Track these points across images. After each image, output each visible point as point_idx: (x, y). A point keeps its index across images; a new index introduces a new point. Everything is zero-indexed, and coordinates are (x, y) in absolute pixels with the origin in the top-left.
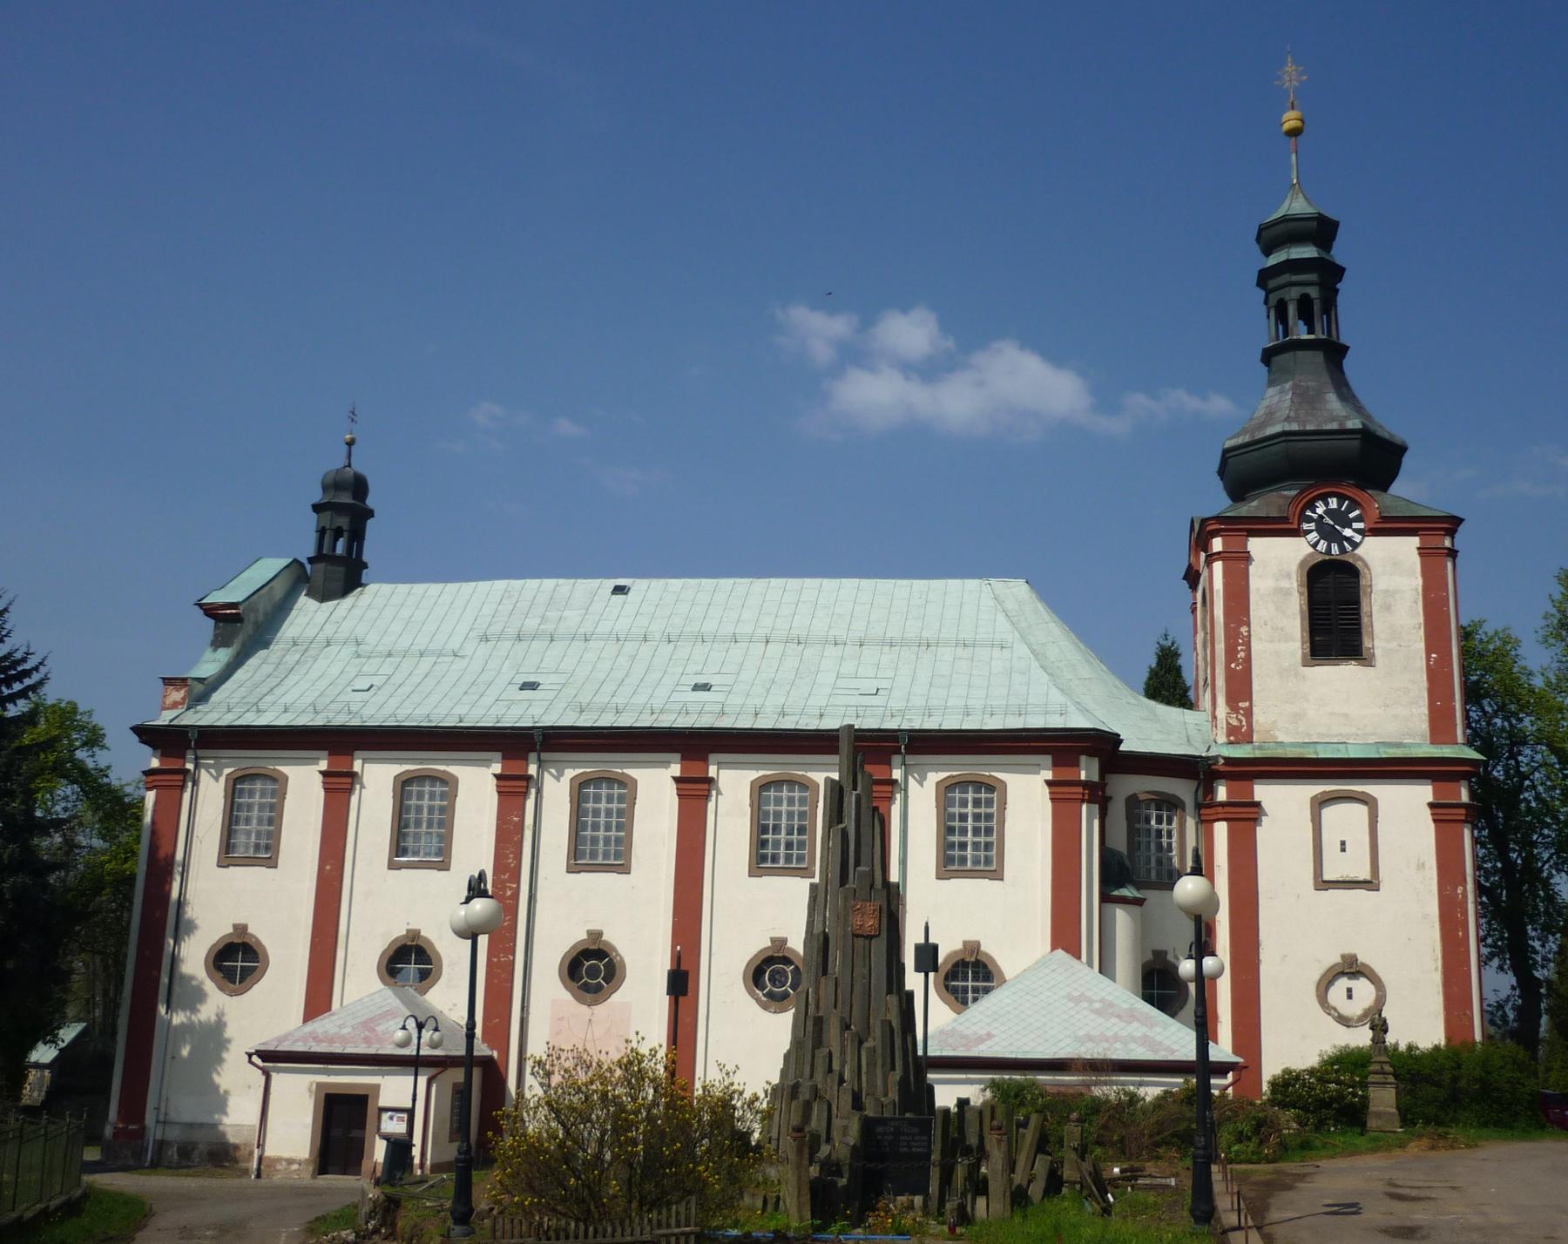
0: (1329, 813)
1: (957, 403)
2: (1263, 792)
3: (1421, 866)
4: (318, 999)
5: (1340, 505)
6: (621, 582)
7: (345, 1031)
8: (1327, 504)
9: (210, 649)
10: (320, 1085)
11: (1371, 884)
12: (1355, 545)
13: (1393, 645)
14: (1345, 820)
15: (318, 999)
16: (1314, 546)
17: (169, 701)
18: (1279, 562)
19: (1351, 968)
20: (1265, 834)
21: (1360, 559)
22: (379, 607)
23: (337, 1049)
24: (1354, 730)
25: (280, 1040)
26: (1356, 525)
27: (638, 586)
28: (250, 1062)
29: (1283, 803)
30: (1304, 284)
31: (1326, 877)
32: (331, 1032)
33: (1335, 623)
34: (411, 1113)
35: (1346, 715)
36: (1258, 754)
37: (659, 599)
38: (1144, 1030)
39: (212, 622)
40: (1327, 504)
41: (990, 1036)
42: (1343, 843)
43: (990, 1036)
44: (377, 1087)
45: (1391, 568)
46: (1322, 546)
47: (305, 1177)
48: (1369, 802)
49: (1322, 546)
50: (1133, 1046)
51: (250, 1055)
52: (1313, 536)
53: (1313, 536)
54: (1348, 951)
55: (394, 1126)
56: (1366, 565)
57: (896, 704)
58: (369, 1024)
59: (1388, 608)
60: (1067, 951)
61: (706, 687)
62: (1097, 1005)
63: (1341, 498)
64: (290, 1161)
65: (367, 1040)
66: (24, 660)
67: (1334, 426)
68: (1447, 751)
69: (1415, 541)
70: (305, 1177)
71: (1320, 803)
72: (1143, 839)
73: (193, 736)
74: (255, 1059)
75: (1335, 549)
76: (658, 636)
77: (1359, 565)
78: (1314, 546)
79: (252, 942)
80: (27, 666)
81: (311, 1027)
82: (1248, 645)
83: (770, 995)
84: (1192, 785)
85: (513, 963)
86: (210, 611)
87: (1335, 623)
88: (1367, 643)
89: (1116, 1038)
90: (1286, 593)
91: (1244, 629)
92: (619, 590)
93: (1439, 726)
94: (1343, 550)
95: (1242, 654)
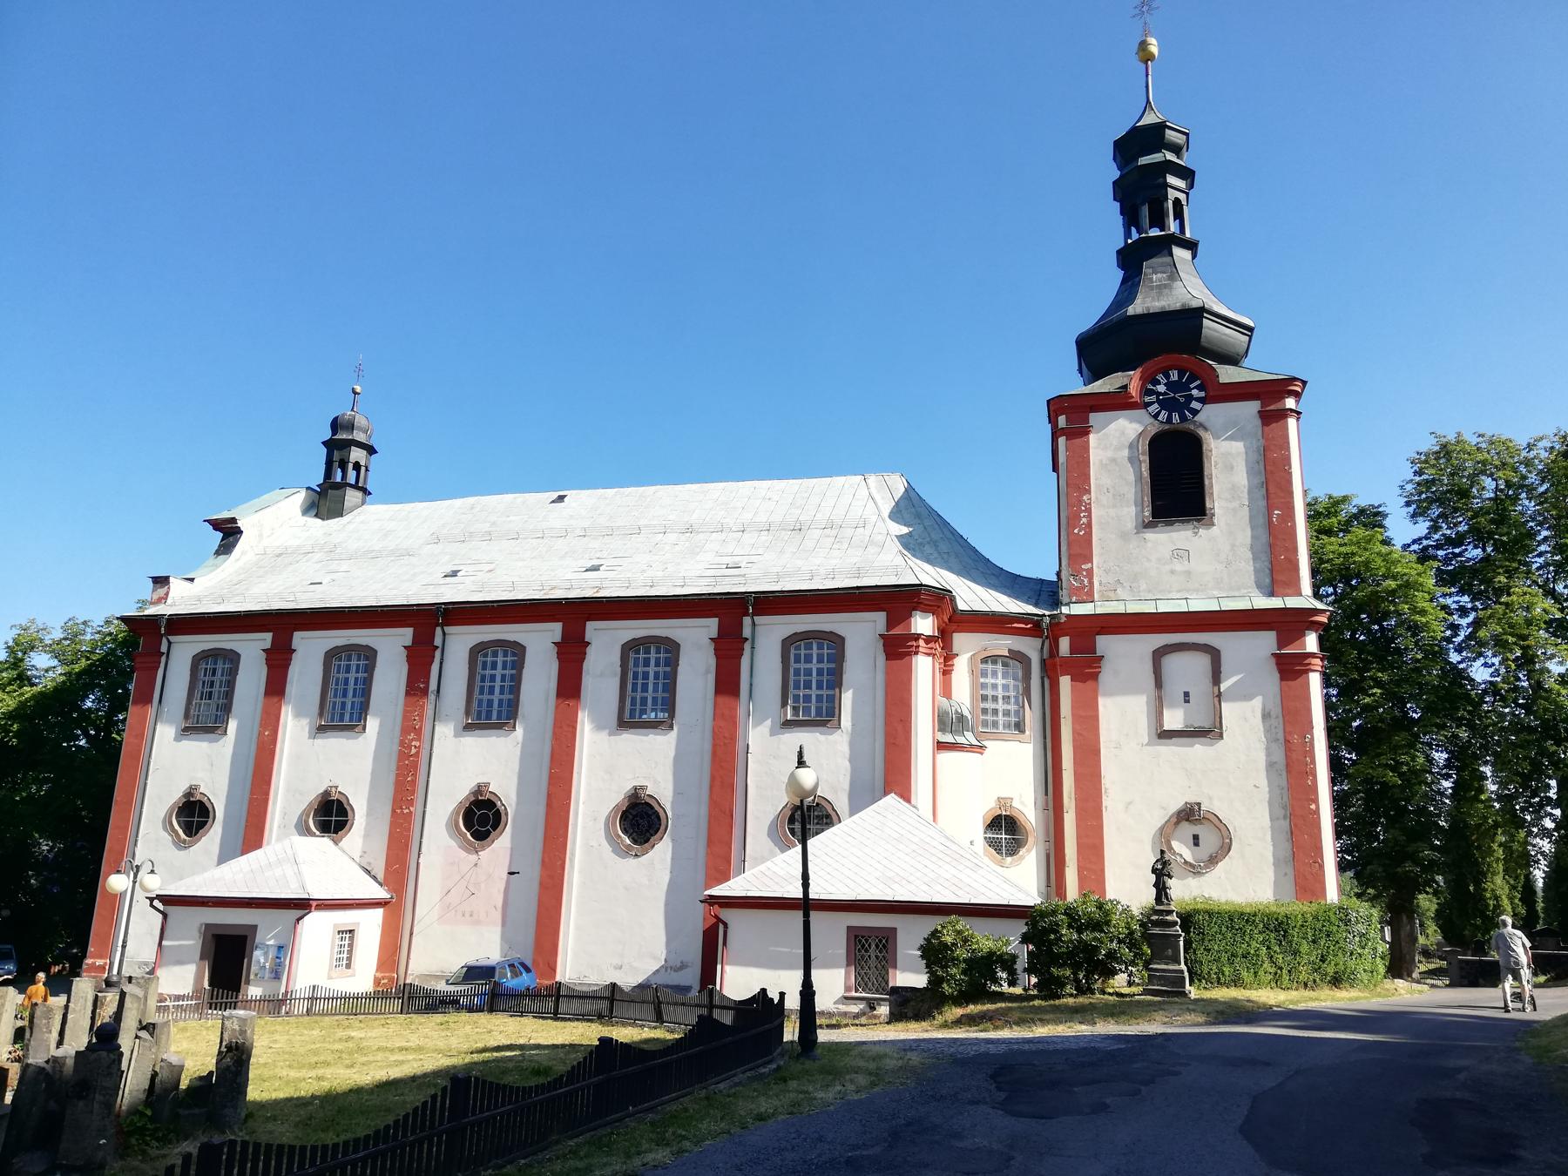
0: (1172, 663)
1: (1520, 950)
2: (1104, 643)
8: (1167, 377)
12: (1195, 412)
14: (1187, 670)
16: (1156, 416)
18: (1117, 442)
19: (1189, 814)
20: (954, 676)
21: (1201, 425)
22: (365, 521)
27: (572, 496)
28: (152, 905)
30: (1145, 175)
33: (1176, 489)
39: (220, 535)
40: (1167, 377)
44: (253, 929)
46: (1163, 415)
48: (1215, 654)
49: (1163, 415)
51: (151, 900)
52: (1154, 408)
53: (1154, 408)
54: (1193, 799)
55: (1206, 565)
60: (902, 796)
61: (595, 568)
68: (1292, 602)
71: (1159, 655)
72: (660, 694)
73: (314, 904)
74: (156, 903)
75: (1176, 418)
78: (1156, 416)
82: (1089, 511)
84: (1037, 642)
87: (1176, 489)
88: (1208, 505)
93: (1278, 575)
94: (1183, 419)
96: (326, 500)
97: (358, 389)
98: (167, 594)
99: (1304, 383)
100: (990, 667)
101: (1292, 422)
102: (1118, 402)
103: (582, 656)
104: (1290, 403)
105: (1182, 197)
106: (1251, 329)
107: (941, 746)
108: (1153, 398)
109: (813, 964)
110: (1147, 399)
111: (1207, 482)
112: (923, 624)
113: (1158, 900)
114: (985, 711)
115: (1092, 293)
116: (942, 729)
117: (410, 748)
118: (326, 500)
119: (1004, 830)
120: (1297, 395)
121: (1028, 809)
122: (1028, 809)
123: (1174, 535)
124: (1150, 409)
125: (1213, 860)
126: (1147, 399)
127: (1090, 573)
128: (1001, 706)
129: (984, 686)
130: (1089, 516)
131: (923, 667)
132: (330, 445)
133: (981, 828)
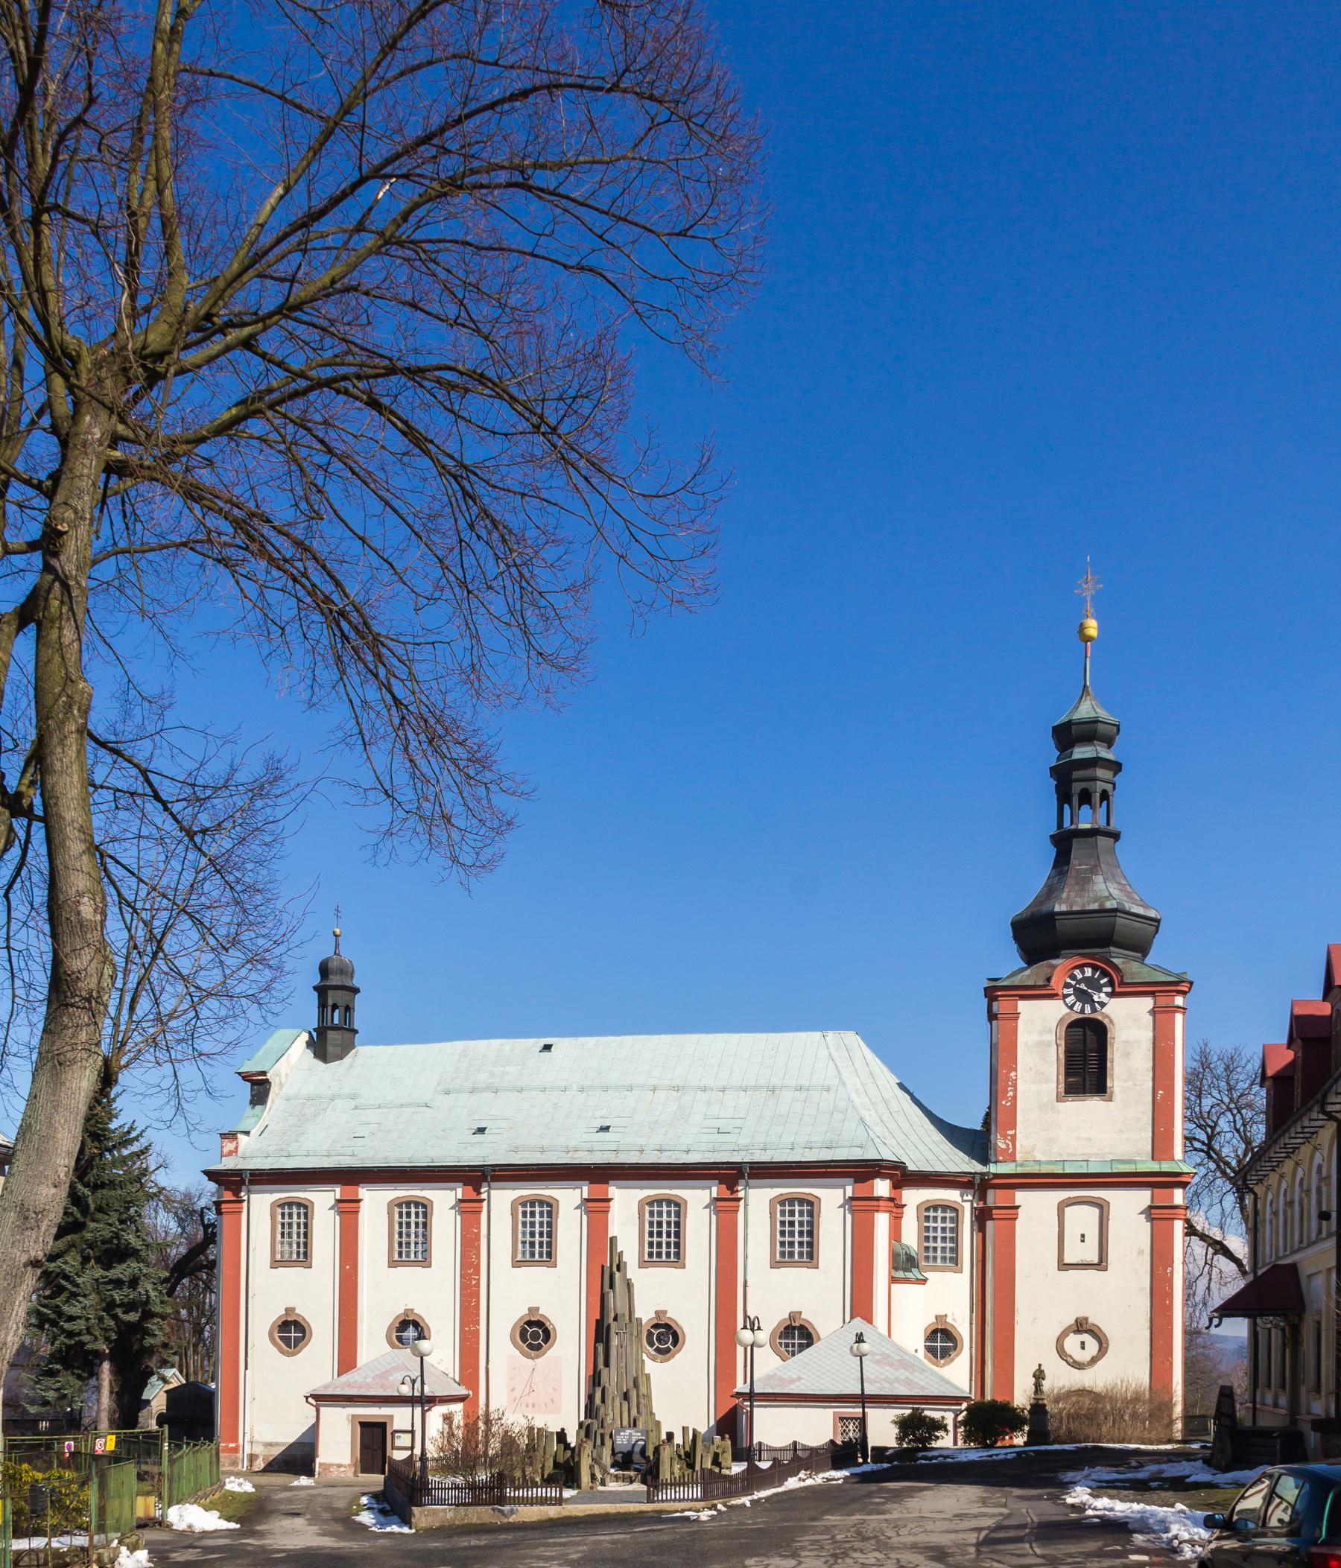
3: (1141, 1252)
4: (347, 1360)
5: (1093, 974)
6: (548, 1041)
7: (368, 1380)
9: (249, 1110)
10: (354, 1416)
11: (1101, 1264)
12: (1103, 1005)
13: (1130, 1084)
15: (347, 1360)
16: (1071, 1007)
17: (226, 1150)
18: (1040, 1026)
19: (1081, 1326)
21: (1107, 1016)
22: (370, 1062)
23: (363, 1392)
24: (1095, 1151)
25: (325, 1387)
26: (1105, 989)
27: (560, 1044)
29: (1035, 1209)
31: (1096, 1261)
32: (354, 1383)
33: (1086, 1065)
34: (412, 1432)
35: (1089, 1139)
36: (1020, 1170)
37: (578, 1055)
38: (907, 1374)
40: (1083, 973)
41: (799, 1378)
42: (1083, 1236)
43: (799, 1378)
45: (1128, 1020)
46: (1078, 1007)
47: (349, 1474)
48: (1102, 1207)
49: (1078, 1007)
50: (896, 1385)
52: (1070, 1000)
53: (1070, 1000)
56: (1111, 1021)
57: (744, 1141)
58: (384, 1375)
59: (1127, 1055)
62: (878, 1357)
63: (1095, 968)
64: (339, 1466)
65: (383, 1386)
66: (129, 1132)
67: (1095, 906)
68: (1166, 1167)
69: (1148, 1003)
70: (349, 1474)
71: (1062, 1207)
73: (247, 1177)
75: (1088, 1009)
76: (575, 1087)
77: (1106, 1022)
79: (300, 1320)
80: (133, 1134)
81: (344, 1378)
82: (1015, 1086)
83: (658, 1350)
85: (478, 1331)
86: (245, 1077)
87: (1086, 1065)
88: (1109, 1084)
89: (897, 1380)
90: (1049, 1044)
91: (1013, 1074)
92: (547, 1048)
94: (1094, 1010)
95: (1011, 1094)
96: (329, 1040)
97: (338, 931)
98: (236, 1148)
99: (1191, 983)
100: (931, 1214)
101: (1179, 1018)
102: (1041, 992)
103: (23, 606)
104: (1179, 1001)
105: (1109, 787)
106: (1158, 921)
107: (893, 1280)
108: (1071, 991)
109: (1246, 1352)
110: (1066, 991)
111: (1109, 1064)
112: (882, 1187)
113: (1036, 1392)
114: (927, 1249)
115: (1025, 877)
116: (896, 1269)
117: (470, 1280)
118: (329, 1040)
119: (941, 1340)
120: (1184, 993)
121: (962, 1325)
122: (962, 1325)
123: (1117, 1069)
124: (1068, 1000)
125: (1094, 1361)
126: (1066, 991)
127: (1014, 1138)
128: (939, 1244)
129: (927, 1229)
130: (1015, 1091)
131: (882, 1221)
132: (321, 991)
133: (923, 1339)
